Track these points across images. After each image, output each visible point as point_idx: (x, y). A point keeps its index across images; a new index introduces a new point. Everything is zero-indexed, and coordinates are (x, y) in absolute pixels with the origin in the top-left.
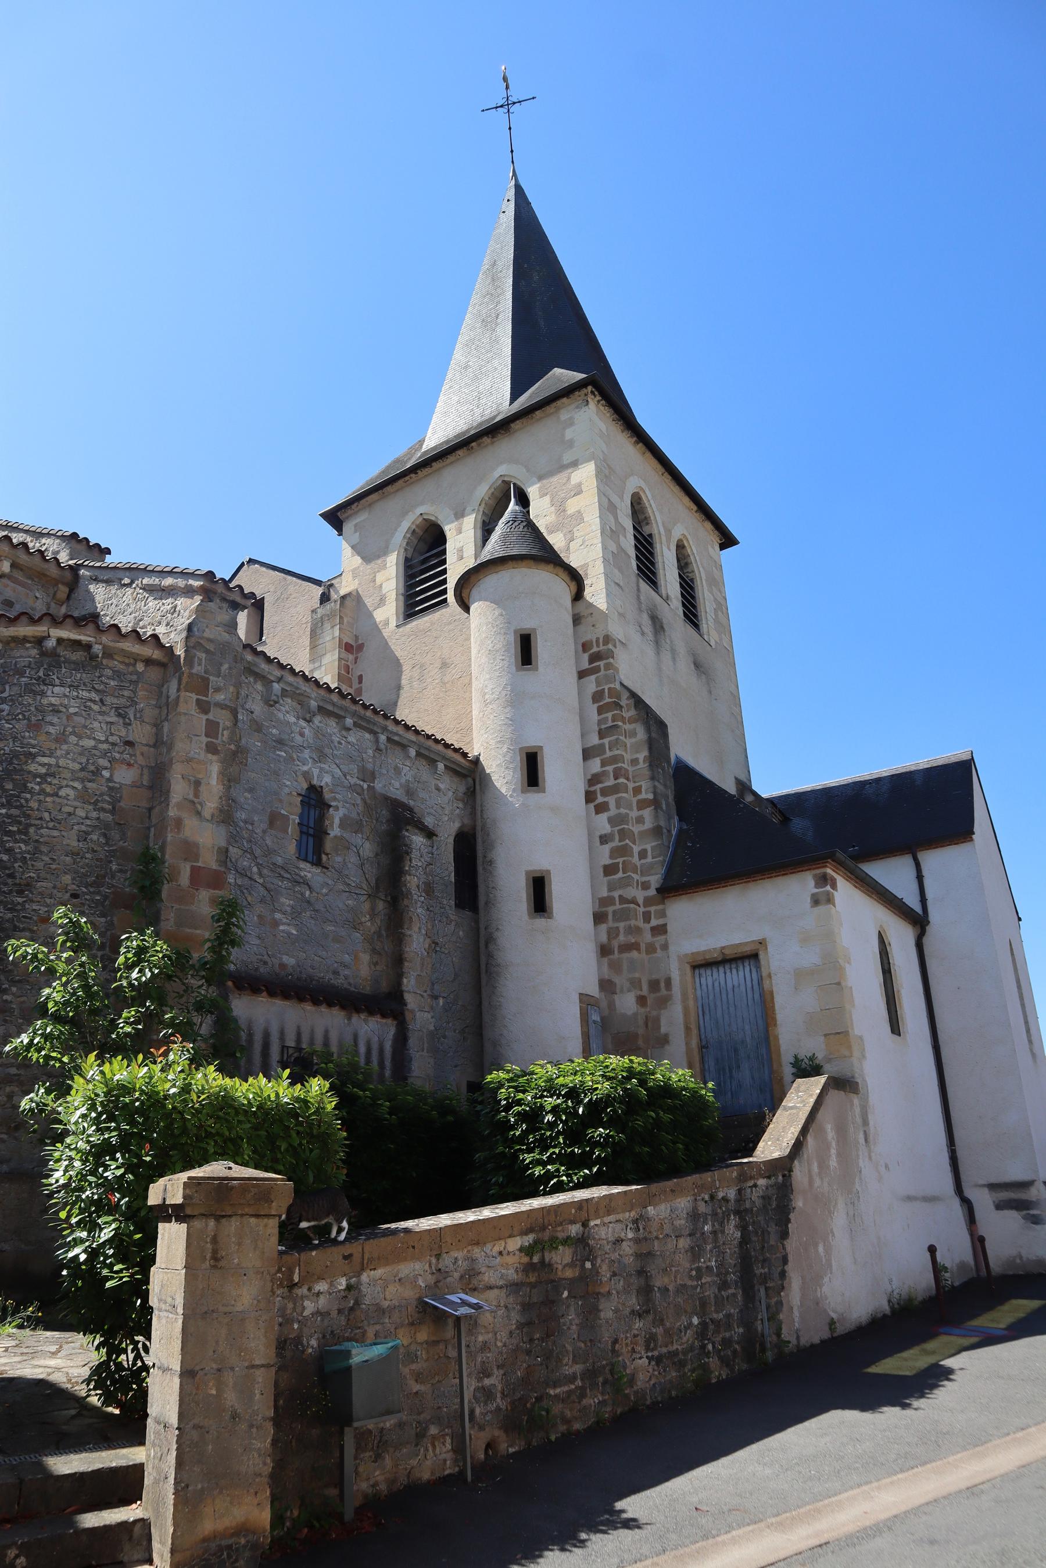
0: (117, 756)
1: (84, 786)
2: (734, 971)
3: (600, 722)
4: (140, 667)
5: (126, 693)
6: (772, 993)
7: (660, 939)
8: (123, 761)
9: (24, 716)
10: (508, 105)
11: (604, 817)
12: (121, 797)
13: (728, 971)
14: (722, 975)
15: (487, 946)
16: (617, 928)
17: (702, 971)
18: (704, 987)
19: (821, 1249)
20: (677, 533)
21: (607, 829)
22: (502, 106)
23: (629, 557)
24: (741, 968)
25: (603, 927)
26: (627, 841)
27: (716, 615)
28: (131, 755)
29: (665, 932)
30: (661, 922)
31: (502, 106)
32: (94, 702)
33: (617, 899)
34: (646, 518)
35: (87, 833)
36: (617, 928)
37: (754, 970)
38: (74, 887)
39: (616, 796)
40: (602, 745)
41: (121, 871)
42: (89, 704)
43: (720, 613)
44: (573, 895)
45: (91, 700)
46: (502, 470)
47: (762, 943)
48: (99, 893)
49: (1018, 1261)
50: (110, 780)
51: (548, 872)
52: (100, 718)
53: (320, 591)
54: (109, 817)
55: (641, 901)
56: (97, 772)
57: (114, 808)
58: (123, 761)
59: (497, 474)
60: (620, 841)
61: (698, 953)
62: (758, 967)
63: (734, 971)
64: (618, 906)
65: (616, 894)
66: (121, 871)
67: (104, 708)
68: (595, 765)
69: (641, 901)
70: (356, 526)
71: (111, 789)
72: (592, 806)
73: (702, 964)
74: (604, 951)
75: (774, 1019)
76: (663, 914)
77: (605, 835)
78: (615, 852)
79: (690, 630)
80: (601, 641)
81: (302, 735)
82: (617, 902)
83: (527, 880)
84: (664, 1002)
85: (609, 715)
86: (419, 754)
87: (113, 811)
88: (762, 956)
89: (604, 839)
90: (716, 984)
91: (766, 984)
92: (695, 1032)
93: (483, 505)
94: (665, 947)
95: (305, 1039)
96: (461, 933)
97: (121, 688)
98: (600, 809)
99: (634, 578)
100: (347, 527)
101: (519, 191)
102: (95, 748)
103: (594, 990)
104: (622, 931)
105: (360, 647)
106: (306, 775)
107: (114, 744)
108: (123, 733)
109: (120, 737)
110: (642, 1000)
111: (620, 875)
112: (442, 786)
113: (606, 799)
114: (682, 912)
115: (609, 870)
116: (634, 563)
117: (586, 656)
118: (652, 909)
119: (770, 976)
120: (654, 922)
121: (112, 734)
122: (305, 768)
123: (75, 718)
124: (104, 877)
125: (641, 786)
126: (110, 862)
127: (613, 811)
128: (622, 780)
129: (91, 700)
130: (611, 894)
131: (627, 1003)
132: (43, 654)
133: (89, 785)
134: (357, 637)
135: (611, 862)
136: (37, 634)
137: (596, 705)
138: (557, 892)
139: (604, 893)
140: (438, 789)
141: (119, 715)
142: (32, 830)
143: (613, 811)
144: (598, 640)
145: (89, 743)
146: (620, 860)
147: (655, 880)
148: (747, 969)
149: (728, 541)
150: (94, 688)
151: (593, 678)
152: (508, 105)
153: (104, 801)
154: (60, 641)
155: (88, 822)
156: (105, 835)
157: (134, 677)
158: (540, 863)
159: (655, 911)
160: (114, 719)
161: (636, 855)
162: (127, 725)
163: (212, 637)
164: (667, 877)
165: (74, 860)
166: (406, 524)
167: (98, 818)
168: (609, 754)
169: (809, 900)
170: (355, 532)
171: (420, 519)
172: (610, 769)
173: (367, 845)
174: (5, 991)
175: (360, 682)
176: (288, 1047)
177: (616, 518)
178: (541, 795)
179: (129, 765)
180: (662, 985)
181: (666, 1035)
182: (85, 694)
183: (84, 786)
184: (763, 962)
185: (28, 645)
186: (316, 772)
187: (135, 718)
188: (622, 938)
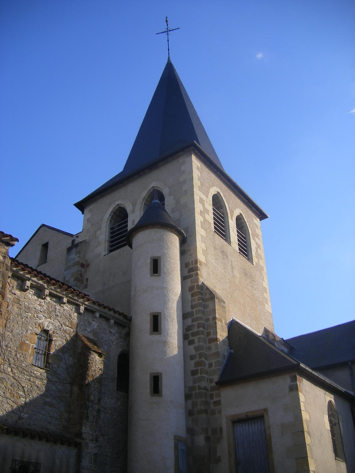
2: (253, 425)
3: (192, 301)
6: (270, 436)
10: (167, 31)
11: (192, 347)
20: (237, 212)
21: (193, 352)
22: (165, 32)
23: (210, 223)
25: (190, 401)
26: (203, 359)
27: (257, 250)
31: (165, 32)
33: (197, 387)
34: (221, 206)
39: (198, 337)
40: (192, 312)
43: (259, 249)
44: (174, 386)
46: (153, 184)
47: (266, 410)
51: (161, 374)
55: (209, 388)
59: (151, 186)
60: (199, 358)
63: (253, 425)
64: (197, 391)
65: (196, 385)
68: (189, 321)
69: (209, 388)
70: (90, 210)
72: (187, 341)
73: (237, 421)
74: (190, 413)
76: (219, 395)
78: (198, 364)
80: (194, 262)
83: (150, 377)
85: (196, 297)
86: (101, 316)
88: (265, 417)
89: (192, 358)
94: (220, 412)
96: (119, 403)
98: (191, 343)
105: (88, 265)
110: (208, 439)
111: (199, 375)
112: (113, 331)
113: (193, 338)
115: (194, 373)
116: (213, 226)
117: (187, 270)
118: (214, 392)
119: (269, 427)
120: (215, 399)
122: (40, 321)
125: (210, 332)
127: (197, 344)
128: (201, 329)
131: (201, 440)
134: (87, 261)
135: (195, 369)
137: (190, 293)
138: (166, 383)
139: (191, 384)
140: (111, 332)
143: (197, 344)
144: (192, 262)
146: (199, 368)
147: (216, 378)
149: (262, 216)
151: (189, 280)
152: (167, 31)
158: (158, 368)
161: (207, 365)
164: (222, 376)
168: (195, 316)
169: (288, 388)
171: (118, 207)
172: (196, 323)
173: (71, 359)
175: (87, 282)
176: (16, 461)
177: (204, 205)
178: (159, 336)
186: (46, 324)
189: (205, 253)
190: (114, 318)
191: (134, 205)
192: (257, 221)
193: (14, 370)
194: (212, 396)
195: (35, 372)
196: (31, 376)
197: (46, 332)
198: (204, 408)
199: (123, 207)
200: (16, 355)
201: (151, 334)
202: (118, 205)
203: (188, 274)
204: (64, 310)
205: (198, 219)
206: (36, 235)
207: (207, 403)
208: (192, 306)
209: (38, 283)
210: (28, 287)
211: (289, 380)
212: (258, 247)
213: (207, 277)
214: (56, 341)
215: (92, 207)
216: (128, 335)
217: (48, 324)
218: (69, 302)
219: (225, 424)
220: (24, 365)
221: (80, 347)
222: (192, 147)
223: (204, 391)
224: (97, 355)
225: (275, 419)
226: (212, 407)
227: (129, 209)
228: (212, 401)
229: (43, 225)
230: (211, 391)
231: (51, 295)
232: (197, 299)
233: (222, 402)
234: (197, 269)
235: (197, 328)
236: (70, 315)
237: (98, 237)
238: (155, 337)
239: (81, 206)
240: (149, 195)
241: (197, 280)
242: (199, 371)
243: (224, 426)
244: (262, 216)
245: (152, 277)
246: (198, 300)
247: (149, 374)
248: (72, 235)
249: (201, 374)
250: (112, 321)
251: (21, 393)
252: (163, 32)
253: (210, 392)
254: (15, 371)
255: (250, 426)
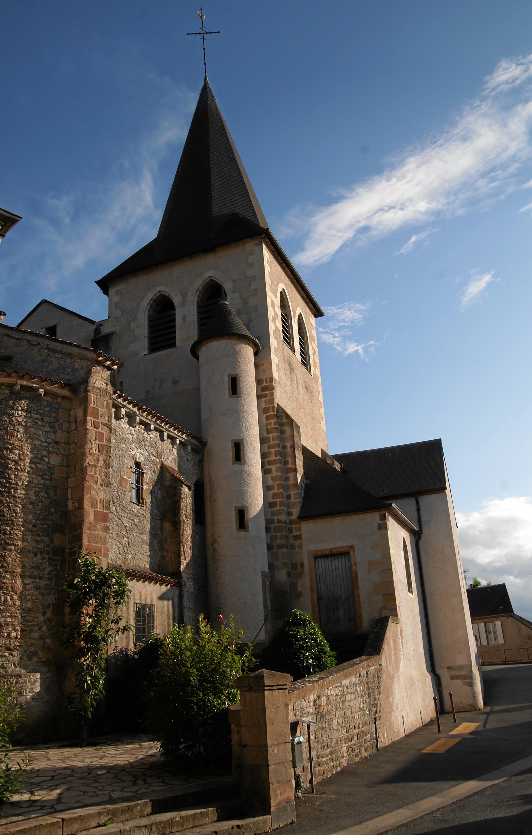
0: (51, 449)
1: (36, 467)
4: (60, 400)
5: (54, 415)
7: (298, 542)
8: (54, 452)
9: (4, 427)
12: (54, 472)
13: (333, 560)
14: (330, 562)
15: (212, 545)
16: (276, 536)
17: (319, 560)
18: (320, 568)
19: (391, 699)
20: (298, 311)
22: (199, 34)
24: (340, 559)
28: (58, 449)
29: (301, 539)
30: (298, 533)
32: (39, 420)
33: (276, 520)
35: (39, 492)
36: (276, 536)
37: (347, 560)
38: (34, 521)
40: (269, 438)
41: (55, 512)
42: (36, 421)
45: (38, 419)
46: (210, 274)
47: (352, 547)
48: (45, 524)
49: (461, 705)
50: (48, 463)
52: (42, 428)
53: (94, 327)
54: (48, 483)
56: (42, 459)
57: (51, 478)
58: (54, 452)
61: (318, 551)
62: (349, 559)
63: (336, 560)
64: (277, 524)
65: (275, 518)
66: (55, 512)
67: (44, 423)
70: (117, 291)
71: (49, 467)
73: (319, 557)
74: (270, 547)
75: (358, 586)
76: (300, 529)
77: (270, 486)
79: (304, 368)
80: (268, 380)
81: (131, 434)
82: (276, 523)
83: (235, 511)
84: (300, 575)
87: (50, 480)
88: (351, 553)
90: (327, 567)
91: (354, 568)
92: (316, 590)
93: (198, 292)
94: (300, 546)
95: (143, 598)
97: (51, 412)
99: (282, 343)
100: (111, 291)
101: (205, 94)
102: (40, 445)
103: (266, 570)
104: (279, 537)
106: (134, 457)
107: (49, 443)
108: (53, 437)
109: (52, 439)
110: (289, 574)
112: (189, 458)
113: (270, 467)
114: (308, 528)
119: (355, 564)
120: (295, 533)
121: (48, 438)
122: (133, 453)
123: (30, 429)
124: (48, 515)
125: (288, 461)
126: (50, 507)
129: (38, 419)
130: (273, 518)
131: (282, 576)
132: (12, 393)
133: (39, 466)
136: (10, 382)
140: (188, 460)
141: (51, 427)
142: (12, 491)
144: (266, 379)
145: (38, 443)
146: (278, 500)
148: (343, 560)
150: (38, 412)
153: (46, 474)
154: (22, 386)
155: (39, 486)
156: (47, 493)
157: (57, 406)
159: (295, 527)
160: (48, 429)
162: (55, 432)
163: (99, 386)
165: (34, 506)
166: (150, 296)
167: (44, 484)
170: (117, 295)
171: (159, 294)
174: (4, 577)
179: (57, 454)
180: (299, 566)
181: (301, 592)
182: (34, 415)
183: (36, 467)
184: (352, 557)
185: (3, 387)
187: (59, 429)
188: (279, 541)
189: (278, 370)
190: (192, 444)
191: (184, 296)
192: (313, 320)
193: (117, 509)
194: (291, 530)
195: (133, 510)
196: (130, 513)
197: (138, 465)
198: (285, 543)
199: (167, 295)
200: (118, 493)
201: (233, 464)
202: (160, 291)
203: (262, 392)
204: (151, 438)
205: (271, 326)
206: (34, 314)
207: (287, 537)
208: (267, 431)
209: (132, 410)
210: (123, 415)
211: (378, 518)
212: (314, 353)
213: (282, 397)
214: (146, 473)
215: (121, 287)
216: (201, 463)
217: (140, 455)
218: (156, 429)
219: (306, 560)
220: (124, 502)
221: (168, 480)
222: (264, 235)
223: (284, 524)
224: (187, 488)
225: (360, 556)
226: (292, 541)
227: (176, 301)
228: (291, 535)
229: (44, 302)
230: (290, 525)
231: (142, 423)
232: (273, 423)
233: (303, 537)
234: (272, 388)
235: (274, 456)
236: (156, 444)
237: (134, 330)
238: (237, 467)
239: (105, 284)
240: (204, 286)
241: (272, 401)
242: (278, 503)
243: (306, 562)
244: (317, 313)
245: (231, 399)
246: (274, 425)
247: (234, 508)
248: (93, 322)
249: (280, 507)
250: (189, 448)
251: (124, 533)
252: (196, 34)
253: (288, 526)
254: (118, 510)
255: (333, 562)
